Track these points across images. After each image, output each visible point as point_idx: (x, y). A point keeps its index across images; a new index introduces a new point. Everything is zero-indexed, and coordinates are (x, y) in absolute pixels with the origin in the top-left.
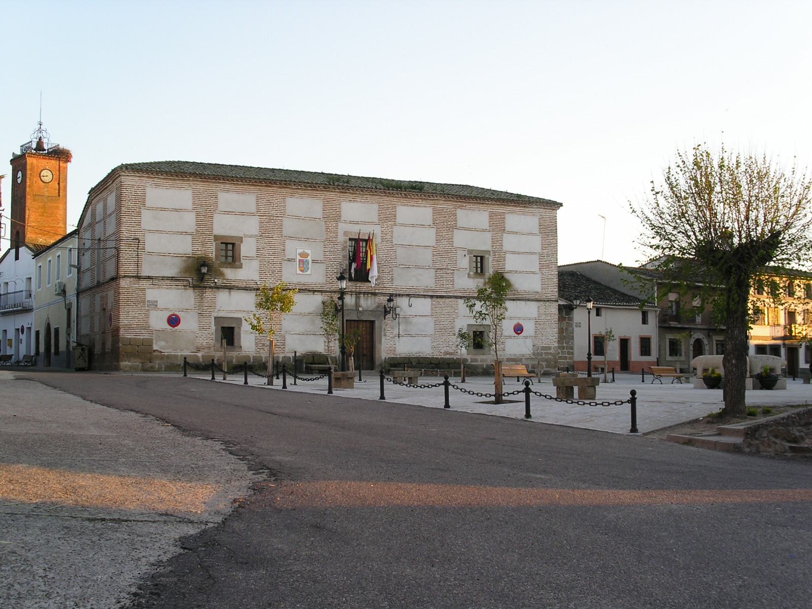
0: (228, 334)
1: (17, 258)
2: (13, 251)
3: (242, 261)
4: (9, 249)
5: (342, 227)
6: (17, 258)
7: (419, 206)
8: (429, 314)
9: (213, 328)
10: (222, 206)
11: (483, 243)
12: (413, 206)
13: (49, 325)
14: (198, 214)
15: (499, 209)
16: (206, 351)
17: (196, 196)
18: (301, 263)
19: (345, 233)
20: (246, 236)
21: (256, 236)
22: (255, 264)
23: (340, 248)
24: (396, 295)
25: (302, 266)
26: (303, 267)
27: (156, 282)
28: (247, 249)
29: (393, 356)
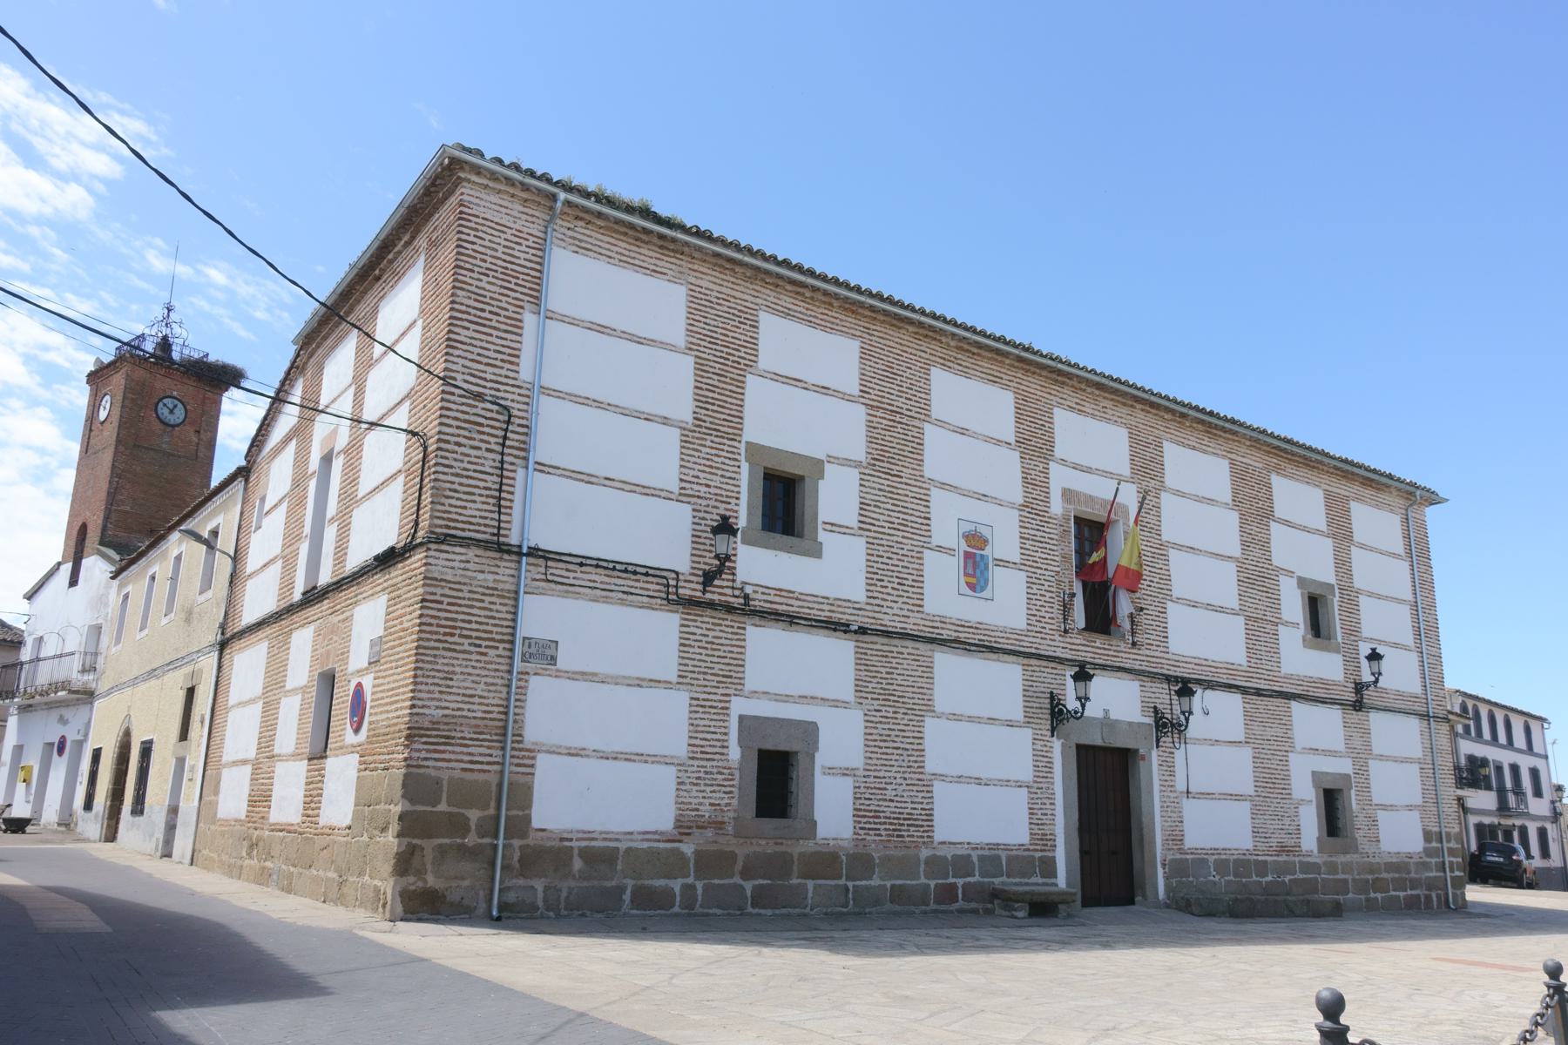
0: (777, 776)
1: (73, 582)
2: (67, 568)
3: (822, 536)
4: (59, 564)
5: (739, 707)
6: (73, 582)
7: (1205, 452)
8: (1242, 739)
9: (735, 753)
10: (767, 358)
11: (1323, 571)
12: (1194, 448)
13: (127, 734)
14: (700, 368)
15: (1342, 488)
16: (709, 833)
17: (697, 307)
18: (970, 562)
19: (1068, 494)
20: (832, 459)
21: (857, 464)
22: (857, 548)
23: (1055, 533)
24: (1198, 682)
25: (970, 571)
26: (974, 576)
27: (557, 569)
28: (835, 499)
29: (1178, 856)
